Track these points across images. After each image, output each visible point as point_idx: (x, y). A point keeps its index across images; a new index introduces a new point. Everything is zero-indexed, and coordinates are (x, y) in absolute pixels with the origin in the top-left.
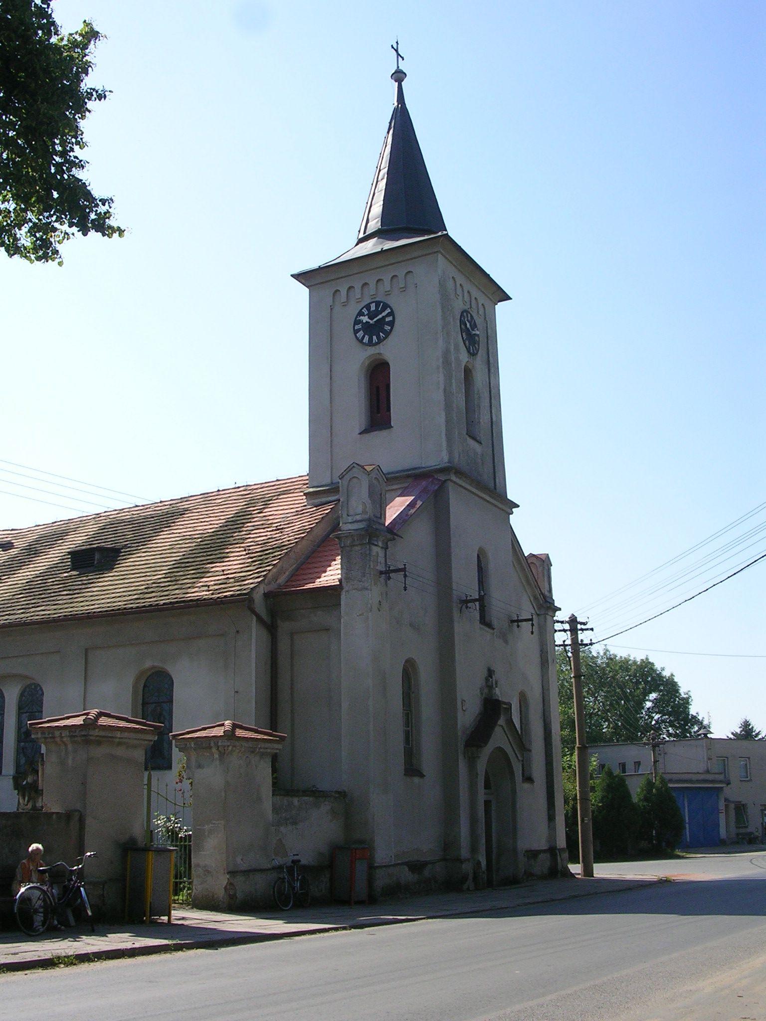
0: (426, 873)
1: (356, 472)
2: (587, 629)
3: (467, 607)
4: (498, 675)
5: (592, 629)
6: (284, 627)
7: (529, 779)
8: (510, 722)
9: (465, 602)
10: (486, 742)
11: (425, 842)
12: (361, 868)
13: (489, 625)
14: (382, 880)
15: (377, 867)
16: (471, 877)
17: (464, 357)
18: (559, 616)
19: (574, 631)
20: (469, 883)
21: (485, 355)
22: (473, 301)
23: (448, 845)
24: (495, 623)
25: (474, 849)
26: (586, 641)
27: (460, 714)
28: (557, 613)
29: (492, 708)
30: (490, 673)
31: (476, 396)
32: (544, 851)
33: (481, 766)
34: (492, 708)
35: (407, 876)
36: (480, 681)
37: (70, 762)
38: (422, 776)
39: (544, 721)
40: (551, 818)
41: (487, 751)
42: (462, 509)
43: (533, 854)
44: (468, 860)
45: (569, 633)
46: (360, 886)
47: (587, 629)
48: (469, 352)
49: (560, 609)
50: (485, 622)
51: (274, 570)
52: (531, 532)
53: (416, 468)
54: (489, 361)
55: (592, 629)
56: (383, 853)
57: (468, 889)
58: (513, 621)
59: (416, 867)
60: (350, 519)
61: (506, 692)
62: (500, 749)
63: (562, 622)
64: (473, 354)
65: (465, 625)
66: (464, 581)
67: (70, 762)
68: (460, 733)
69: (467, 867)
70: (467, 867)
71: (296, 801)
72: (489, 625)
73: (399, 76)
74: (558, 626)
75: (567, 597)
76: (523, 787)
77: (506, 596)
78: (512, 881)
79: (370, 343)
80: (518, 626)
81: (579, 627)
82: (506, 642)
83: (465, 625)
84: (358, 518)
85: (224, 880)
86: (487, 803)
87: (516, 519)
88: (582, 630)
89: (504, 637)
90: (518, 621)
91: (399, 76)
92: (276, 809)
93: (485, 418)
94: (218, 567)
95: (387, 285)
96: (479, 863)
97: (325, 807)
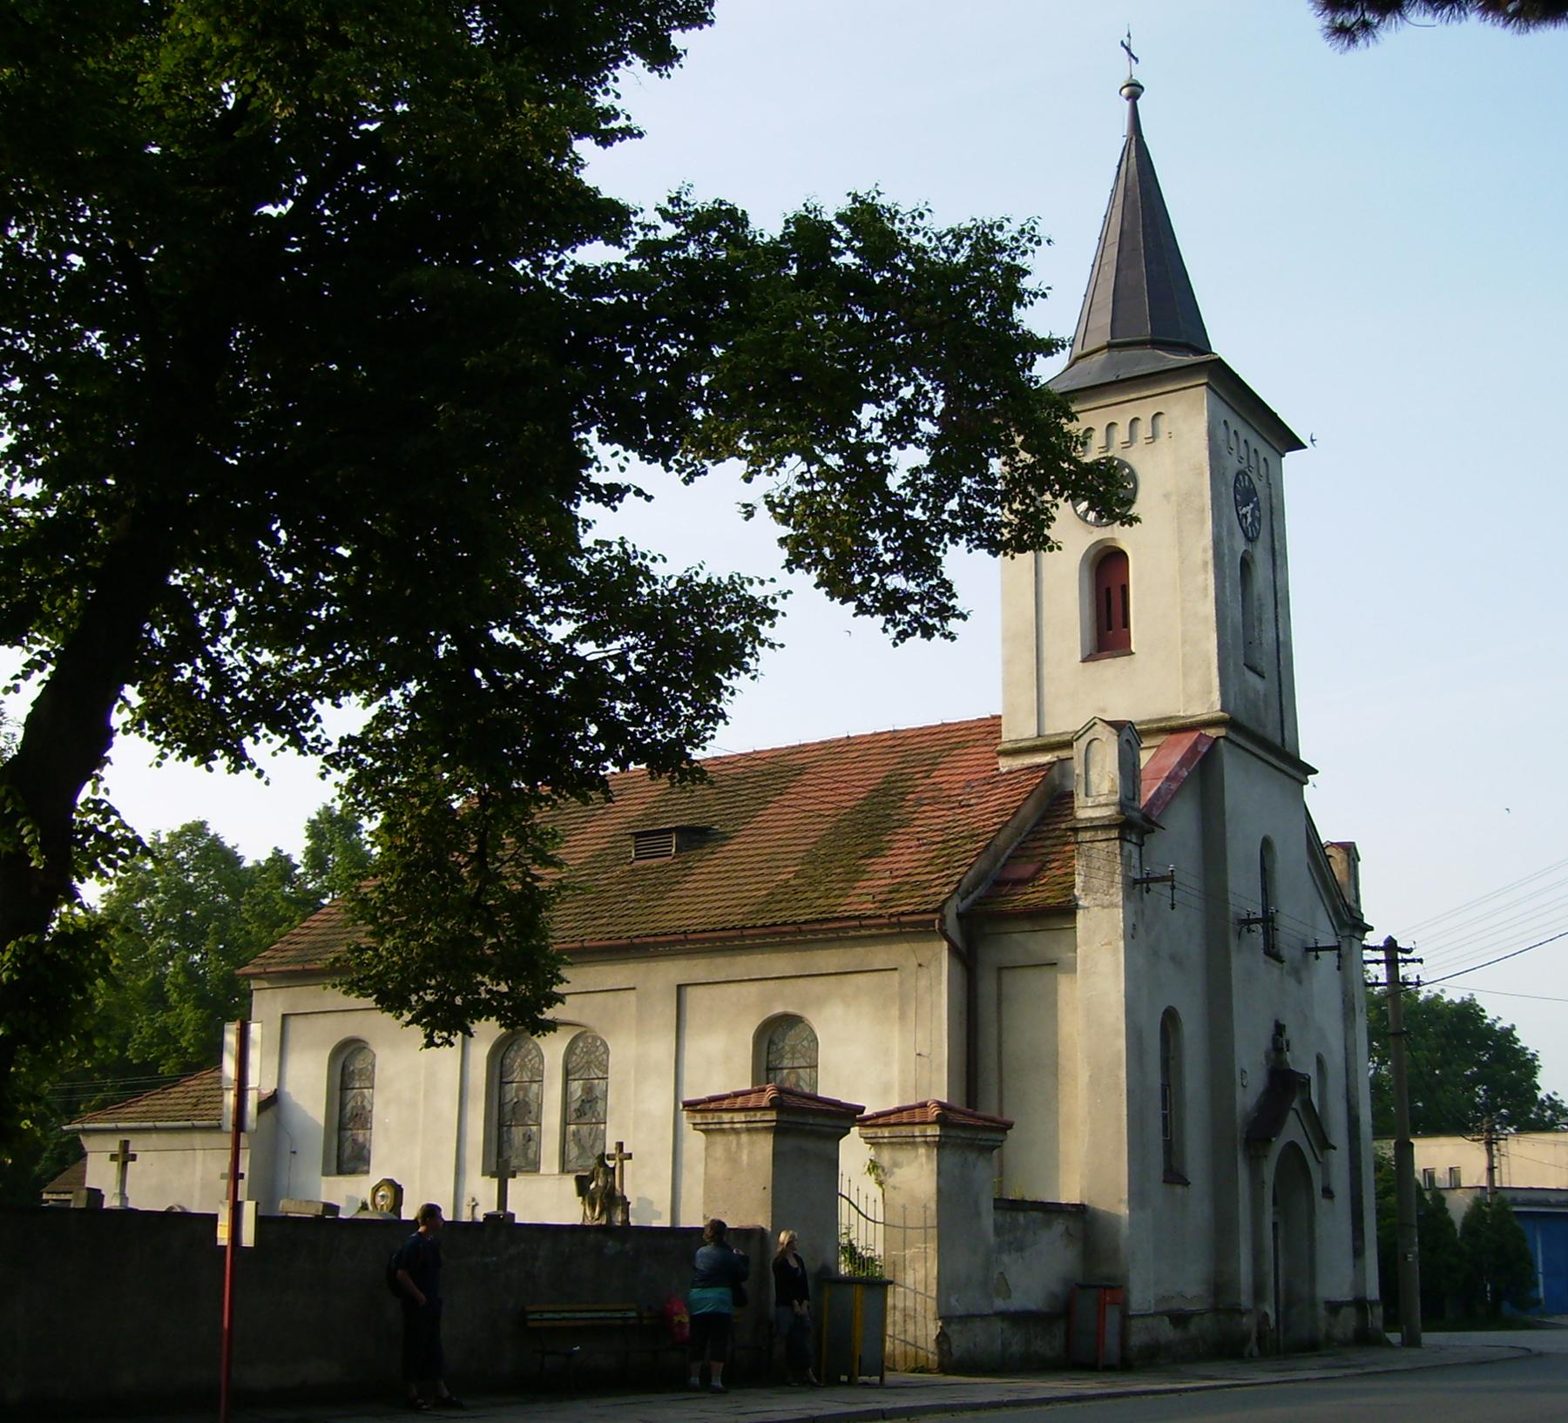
0: (1193, 1328)
1: (1100, 727)
2: (1413, 961)
3: (1249, 930)
4: (1291, 1033)
5: (1421, 961)
6: (990, 956)
7: (1328, 1193)
8: (1307, 1104)
9: (1247, 922)
10: (1277, 1133)
11: (1190, 1283)
12: (1113, 1316)
13: (1278, 958)
14: (1137, 1339)
15: (1133, 1316)
16: (1254, 1337)
17: (1240, 545)
18: (1371, 939)
19: (1392, 964)
20: (1252, 1345)
21: (1268, 539)
22: (1252, 455)
23: (1220, 1286)
24: (1285, 952)
25: (1258, 1293)
26: (1413, 979)
27: (1239, 1090)
28: (1368, 934)
29: (1284, 1084)
30: (1279, 1029)
31: (1256, 604)
32: (1348, 1304)
33: (1269, 1170)
34: (1284, 1084)
35: (1167, 1331)
36: (1265, 1042)
37: (745, 1157)
38: (1186, 1183)
39: (1348, 1101)
40: (1358, 1252)
41: (1278, 1144)
42: (1243, 784)
43: (1334, 1307)
44: (1249, 1311)
45: (1383, 966)
46: (1111, 1342)
47: (1413, 961)
48: (1246, 535)
49: (1371, 929)
50: (1272, 952)
51: (971, 873)
52: (1332, 809)
53: (1171, 718)
54: (1273, 548)
55: (1421, 961)
56: (1141, 1296)
57: (1251, 1355)
58: (1308, 950)
59: (1180, 1319)
60: (1090, 802)
61: (1301, 1061)
62: (1292, 1146)
63: (1374, 949)
64: (1250, 540)
65: (1246, 959)
66: (1244, 894)
67: (745, 1157)
68: (1239, 1121)
69: (1249, 1323)
70: (1249, 1323)
71: (1021, 1218)
72: (1278, 958)
73: (1134, 91)
74: (1368, 955)
75: (1382, 911)
76: (1321, 1203)
77: (1302, 916)
78: (1310, 1347)
79: (1098, 523)
80: (1317, 957)
81: (1400, 955)
82: (1300, 982)
83: (1246, 959)
84: (1102, 800)
85: (933, 1329)
86: (1275, 1225)
87: (1314, 795)
88: (1406, 961)
89: (1297, 974)
90: (1317, 949)
91: (1134, 91)
92: (998, 1230)
93: (1269, 636)
94: (878, 864)
95: (1121, 434)
96: (1266, 1314)
97: (1059, 1226)
